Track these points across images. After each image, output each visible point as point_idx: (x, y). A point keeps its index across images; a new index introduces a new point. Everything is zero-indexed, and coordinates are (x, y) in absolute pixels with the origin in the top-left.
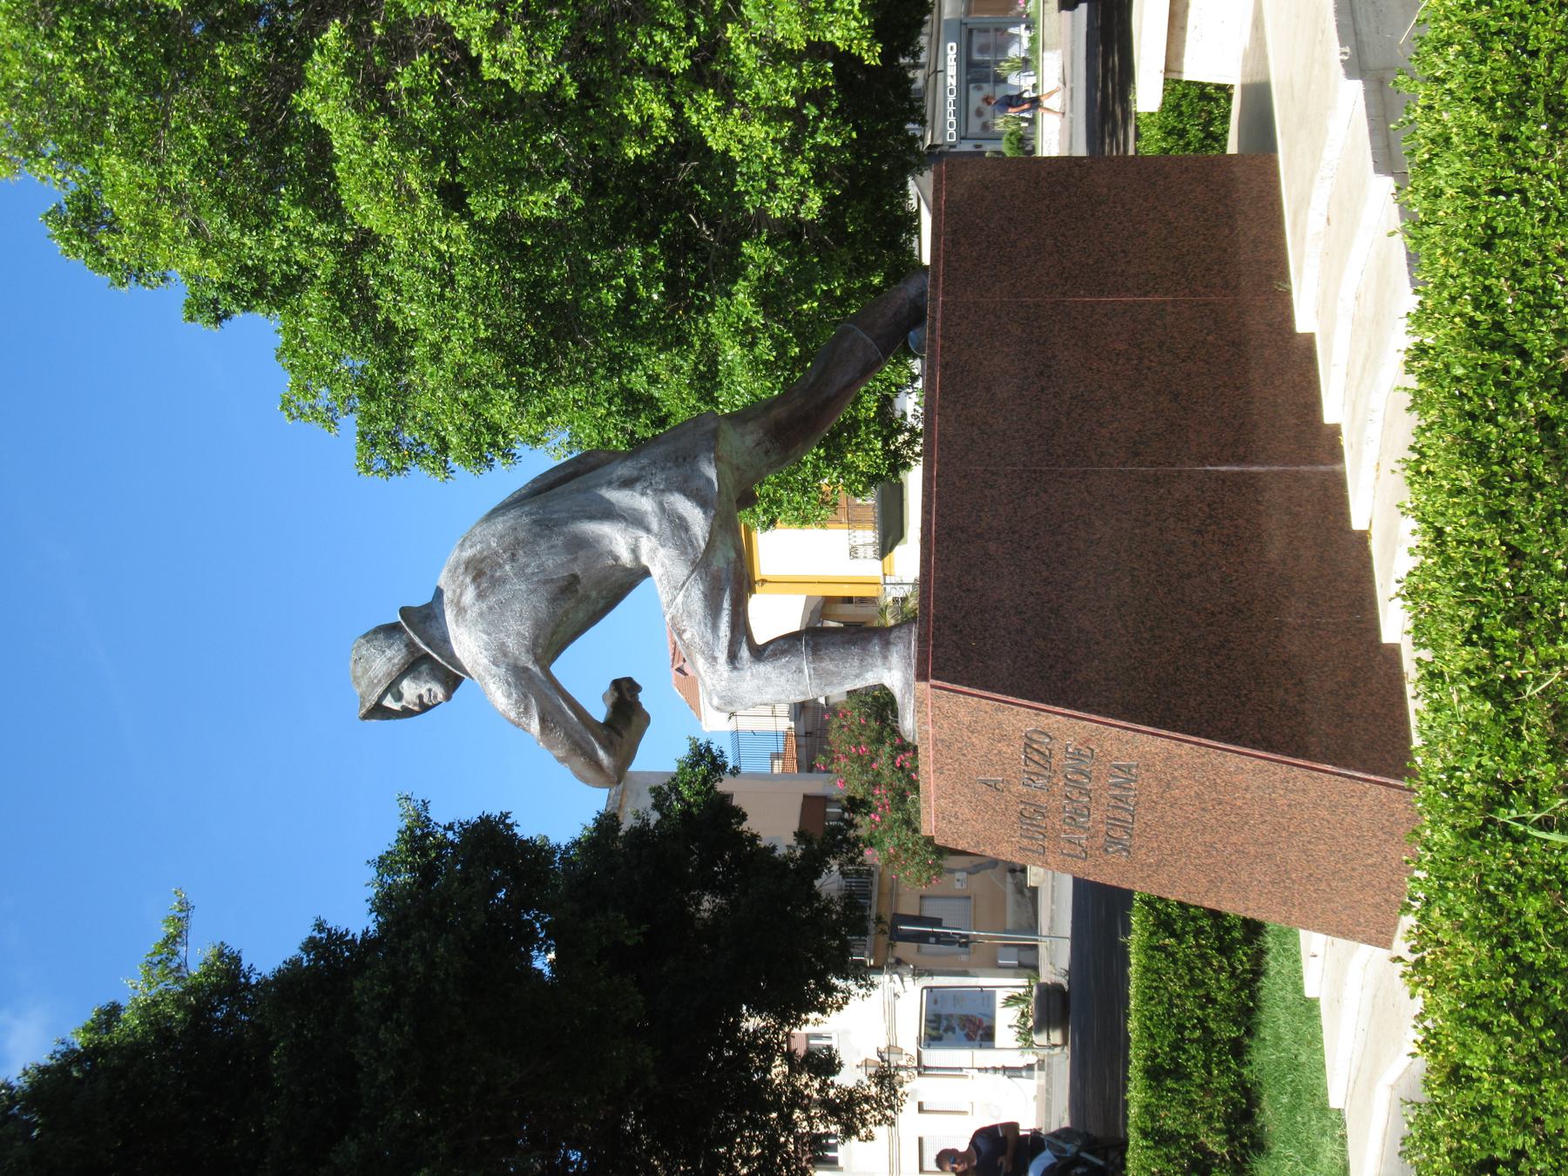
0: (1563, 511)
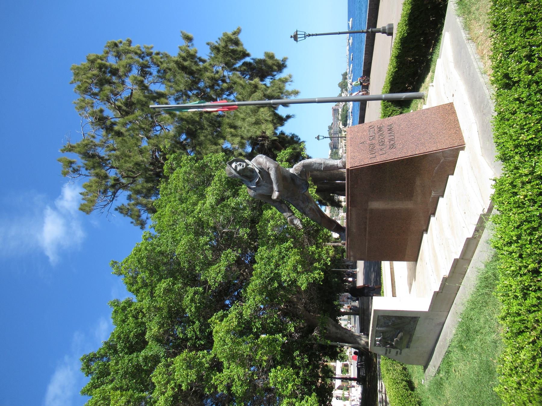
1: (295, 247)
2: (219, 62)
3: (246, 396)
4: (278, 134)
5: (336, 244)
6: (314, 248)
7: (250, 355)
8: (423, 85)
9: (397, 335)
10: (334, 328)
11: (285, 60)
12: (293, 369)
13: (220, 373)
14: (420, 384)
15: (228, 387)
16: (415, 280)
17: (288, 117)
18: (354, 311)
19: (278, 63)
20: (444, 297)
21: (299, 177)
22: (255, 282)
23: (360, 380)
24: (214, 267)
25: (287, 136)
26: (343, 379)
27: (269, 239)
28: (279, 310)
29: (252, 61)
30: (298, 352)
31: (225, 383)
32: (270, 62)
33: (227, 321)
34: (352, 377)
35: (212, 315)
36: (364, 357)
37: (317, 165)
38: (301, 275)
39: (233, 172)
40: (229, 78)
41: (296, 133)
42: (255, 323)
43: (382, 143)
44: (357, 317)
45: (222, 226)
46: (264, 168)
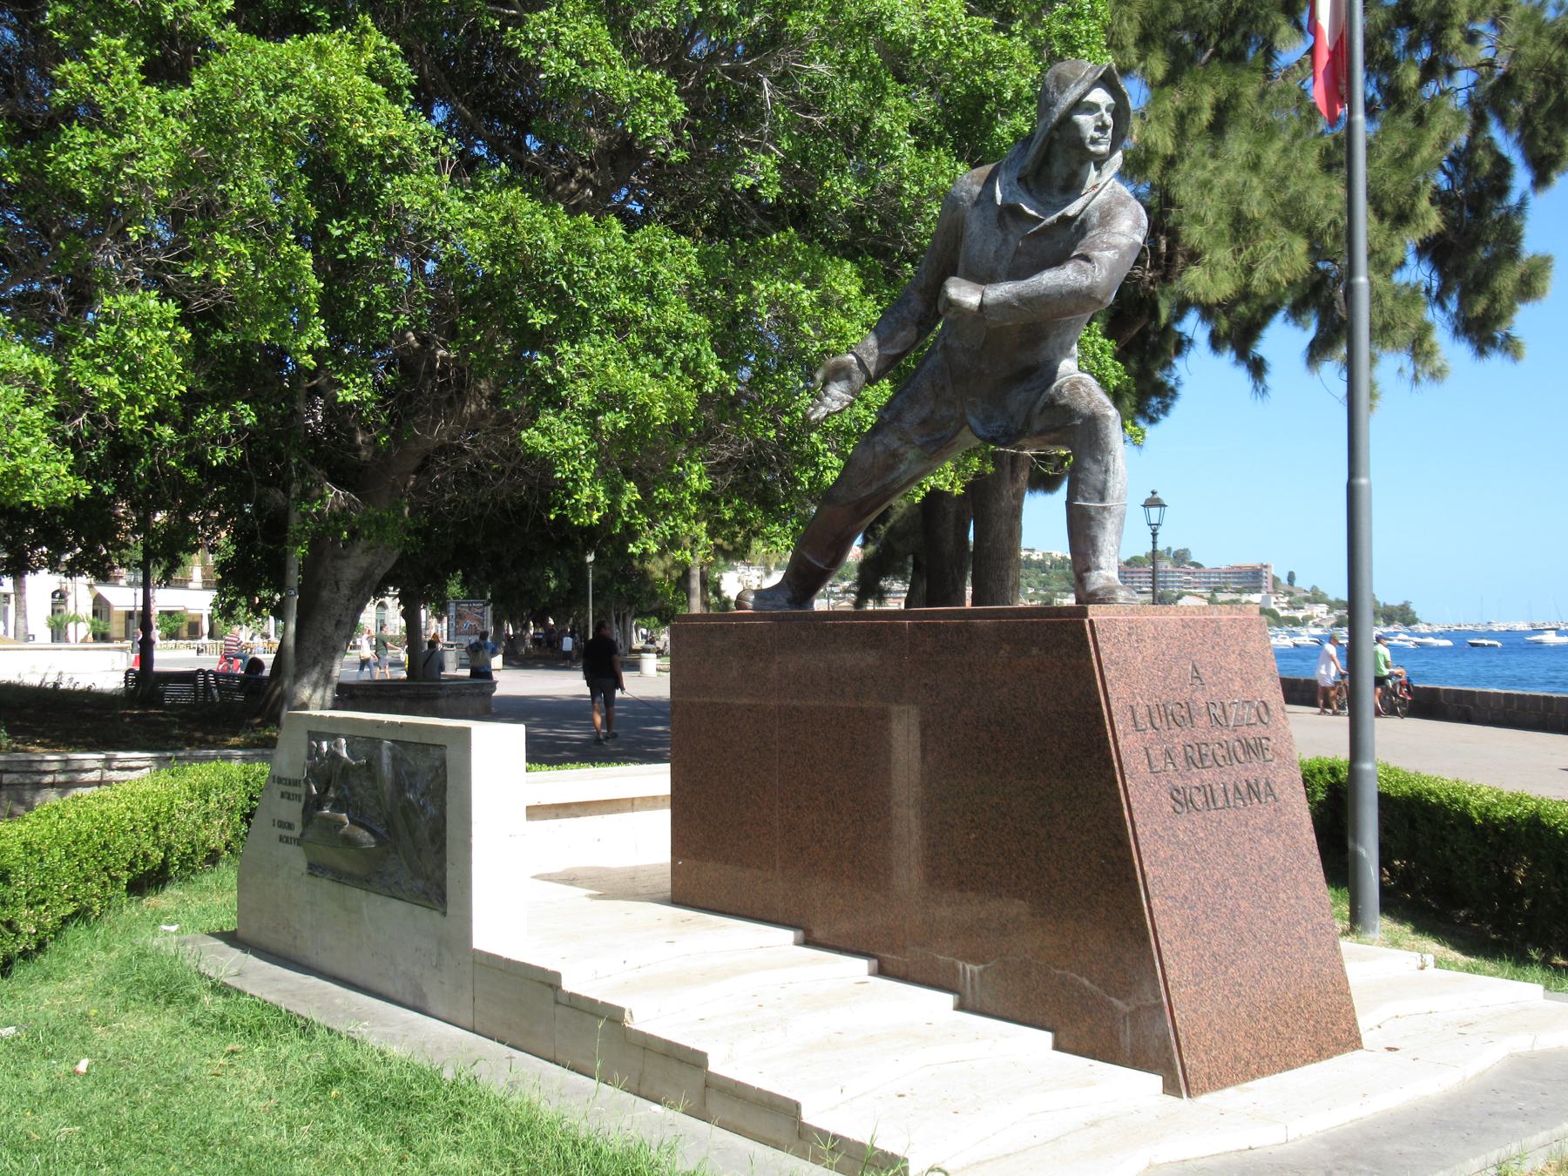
0: (772, 9)
1: (705, 400)
2: (1520, 43)
3: (45, 198)
4: (1179, 328)
5: (695, 584)
6: (697, 478)
7: (226, 206)
8: (1407, 929)
9: (362, 826)
10: (358, 575)
11: (1510, 347)
12: (181, 397)
13: (142, 70)
14: (159, 918)
15: (88, 113)
16: (592, 897)
17: (1257, 368)
18: (424, 659)
19: (1499, 318)
20: (533, 1008)
21: (1044, 398)
22: (545, 228)
23: (146, 681)
24: (604, 36)
25: (1168, 364)
26: (144, 619)
27: (729, 289)
28: (424, 341)
29: (1513, 199)
30: (250, 420)
31: (100, 94)
32: (1506, 281)
33: (371, 100)
34: (158, 655)
35: (392, 35)
36: (240, 698)
37: (1096, 478)
38: (585, 425)
39: (1071, 96)
40: (1443, 93)
41: (1179, 408)
42: (368, 228)
43: (1196, 758)
44: (404, 675)
45: (785, 74)
46: (1087, 240)
